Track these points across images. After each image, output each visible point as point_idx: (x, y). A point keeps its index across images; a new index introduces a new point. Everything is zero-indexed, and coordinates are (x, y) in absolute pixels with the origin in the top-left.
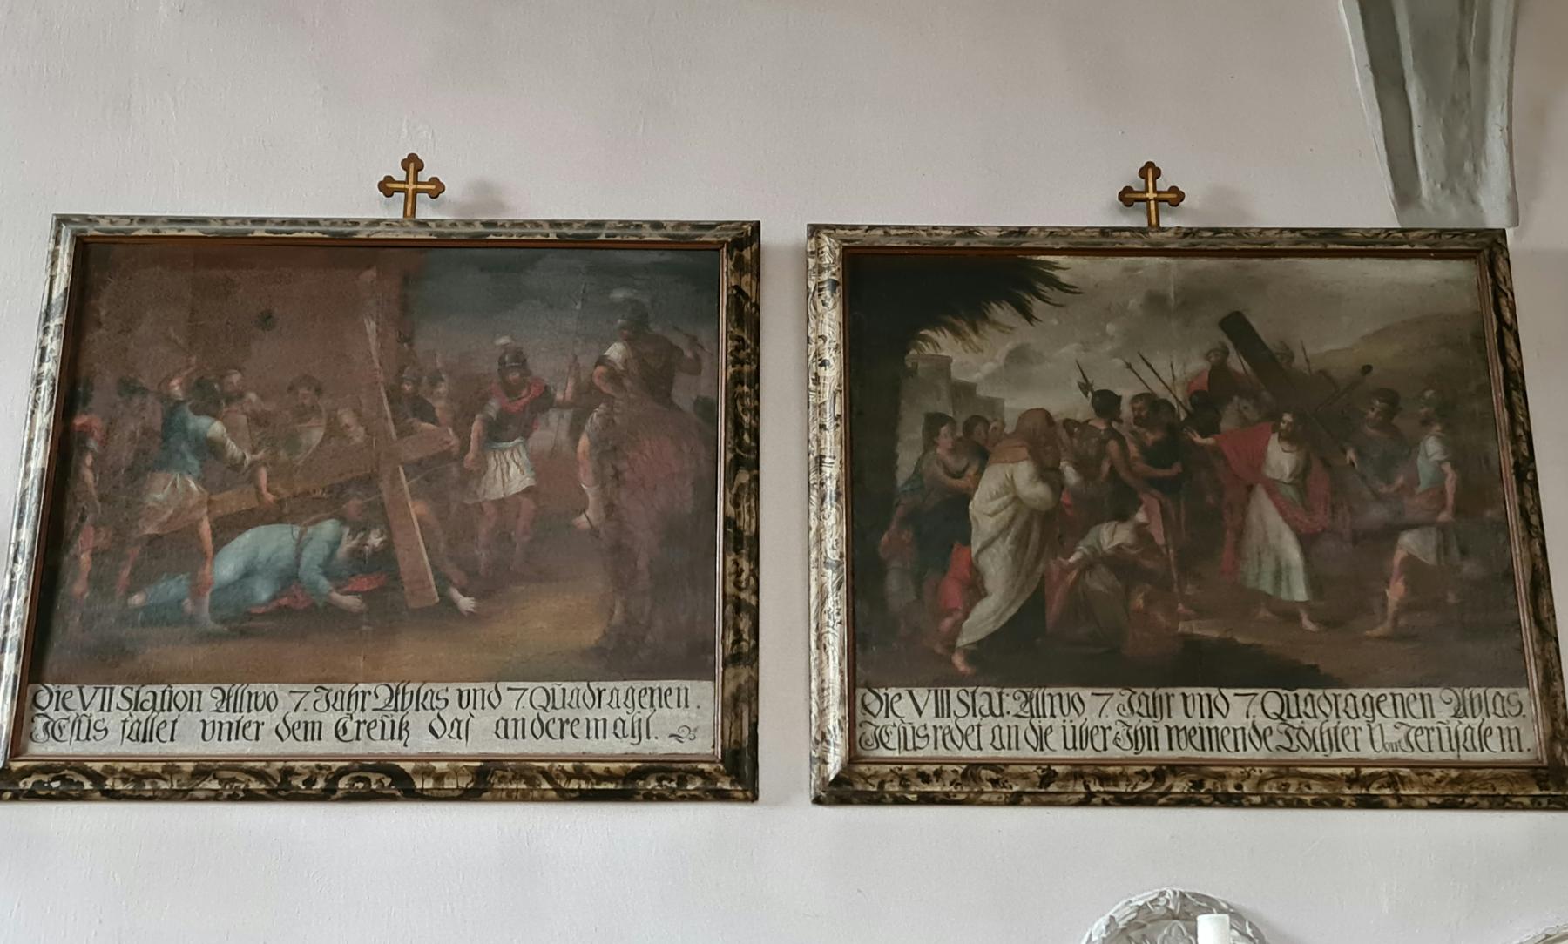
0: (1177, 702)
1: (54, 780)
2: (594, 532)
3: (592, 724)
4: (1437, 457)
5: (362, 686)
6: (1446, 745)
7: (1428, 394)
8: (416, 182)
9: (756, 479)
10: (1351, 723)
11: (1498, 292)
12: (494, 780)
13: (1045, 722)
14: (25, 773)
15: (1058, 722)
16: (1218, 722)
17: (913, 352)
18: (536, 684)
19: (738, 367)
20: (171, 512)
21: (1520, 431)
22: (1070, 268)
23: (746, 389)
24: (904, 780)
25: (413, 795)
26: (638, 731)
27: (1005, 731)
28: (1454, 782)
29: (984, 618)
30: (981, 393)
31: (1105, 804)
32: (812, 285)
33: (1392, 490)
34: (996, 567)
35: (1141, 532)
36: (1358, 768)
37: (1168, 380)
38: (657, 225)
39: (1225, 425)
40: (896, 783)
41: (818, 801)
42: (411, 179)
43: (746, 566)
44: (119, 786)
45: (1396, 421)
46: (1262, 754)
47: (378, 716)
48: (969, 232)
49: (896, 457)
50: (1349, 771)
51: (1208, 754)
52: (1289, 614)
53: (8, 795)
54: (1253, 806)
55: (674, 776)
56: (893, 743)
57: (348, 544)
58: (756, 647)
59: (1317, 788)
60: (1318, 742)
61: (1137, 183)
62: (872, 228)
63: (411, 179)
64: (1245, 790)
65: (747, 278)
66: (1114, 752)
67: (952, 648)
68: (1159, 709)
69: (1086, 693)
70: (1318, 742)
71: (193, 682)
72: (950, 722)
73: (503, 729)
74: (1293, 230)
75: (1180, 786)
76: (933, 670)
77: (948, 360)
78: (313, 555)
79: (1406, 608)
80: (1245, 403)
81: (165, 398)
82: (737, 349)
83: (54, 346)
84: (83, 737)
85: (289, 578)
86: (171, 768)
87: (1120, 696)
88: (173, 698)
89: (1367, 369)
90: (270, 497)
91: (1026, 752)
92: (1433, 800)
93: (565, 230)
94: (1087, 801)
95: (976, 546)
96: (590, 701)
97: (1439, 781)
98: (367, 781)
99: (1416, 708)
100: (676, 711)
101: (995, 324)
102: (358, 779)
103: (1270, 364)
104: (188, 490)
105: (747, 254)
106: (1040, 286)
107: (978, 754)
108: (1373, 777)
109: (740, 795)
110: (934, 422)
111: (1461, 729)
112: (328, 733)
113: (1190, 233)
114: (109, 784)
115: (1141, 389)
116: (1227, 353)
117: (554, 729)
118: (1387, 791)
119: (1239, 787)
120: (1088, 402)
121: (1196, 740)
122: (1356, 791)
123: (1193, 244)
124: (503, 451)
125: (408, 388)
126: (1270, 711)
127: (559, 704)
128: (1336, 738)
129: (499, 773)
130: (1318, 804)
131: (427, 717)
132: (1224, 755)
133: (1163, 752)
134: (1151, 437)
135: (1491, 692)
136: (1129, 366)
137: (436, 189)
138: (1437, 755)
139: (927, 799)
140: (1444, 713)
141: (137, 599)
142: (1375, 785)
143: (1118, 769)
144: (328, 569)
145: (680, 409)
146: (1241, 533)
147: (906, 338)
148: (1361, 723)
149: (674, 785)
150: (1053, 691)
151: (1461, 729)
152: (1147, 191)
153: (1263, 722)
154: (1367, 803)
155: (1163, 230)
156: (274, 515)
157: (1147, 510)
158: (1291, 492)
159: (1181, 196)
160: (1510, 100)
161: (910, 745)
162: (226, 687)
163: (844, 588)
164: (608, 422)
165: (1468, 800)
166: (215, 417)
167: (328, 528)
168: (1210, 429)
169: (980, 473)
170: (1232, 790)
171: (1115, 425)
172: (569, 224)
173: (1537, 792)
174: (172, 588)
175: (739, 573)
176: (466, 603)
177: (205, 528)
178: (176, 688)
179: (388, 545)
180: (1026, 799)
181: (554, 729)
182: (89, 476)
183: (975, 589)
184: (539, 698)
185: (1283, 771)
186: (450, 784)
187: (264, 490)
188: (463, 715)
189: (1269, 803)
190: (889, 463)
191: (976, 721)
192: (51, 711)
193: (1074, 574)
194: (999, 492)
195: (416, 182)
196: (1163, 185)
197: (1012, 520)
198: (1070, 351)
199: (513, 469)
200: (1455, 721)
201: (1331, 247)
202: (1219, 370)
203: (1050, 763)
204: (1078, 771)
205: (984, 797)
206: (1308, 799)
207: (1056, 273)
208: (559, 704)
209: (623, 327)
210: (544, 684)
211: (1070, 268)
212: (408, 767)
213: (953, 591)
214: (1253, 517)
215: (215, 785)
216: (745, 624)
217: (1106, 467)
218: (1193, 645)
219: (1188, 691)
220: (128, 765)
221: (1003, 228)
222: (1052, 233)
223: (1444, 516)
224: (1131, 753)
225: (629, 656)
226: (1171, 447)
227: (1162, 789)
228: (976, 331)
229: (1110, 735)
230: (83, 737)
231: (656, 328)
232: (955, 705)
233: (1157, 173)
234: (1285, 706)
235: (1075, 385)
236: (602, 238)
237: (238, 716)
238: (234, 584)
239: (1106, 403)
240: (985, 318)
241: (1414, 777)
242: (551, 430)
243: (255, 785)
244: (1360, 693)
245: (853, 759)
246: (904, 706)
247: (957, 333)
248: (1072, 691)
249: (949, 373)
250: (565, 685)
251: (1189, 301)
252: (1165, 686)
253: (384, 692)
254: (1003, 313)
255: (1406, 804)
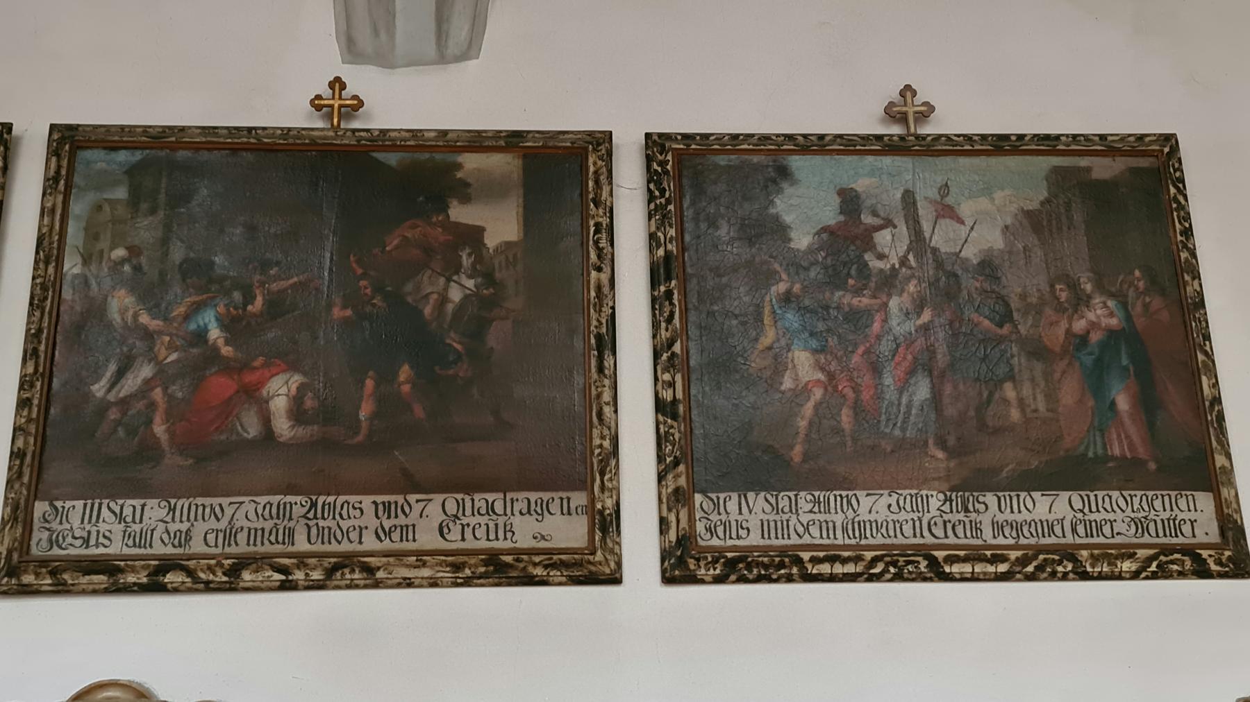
8: (340, 98)
60: (850, 532)
61: (920, 99)
63: (905, 108)
70: (850, 532)
160: (473, 25)
210: (456, 496)
233: (914, 93)
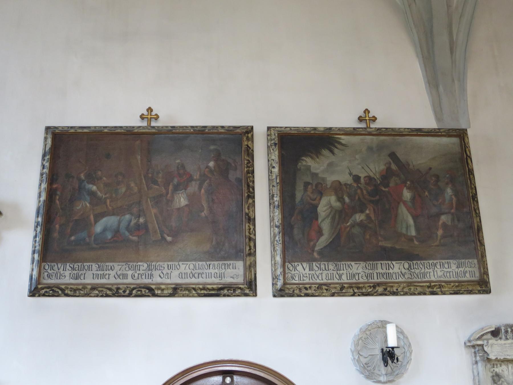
0: (379, 266)
1: (50, 291)
2: (206, 217)
3: (207, 274)
4: (450, 194)
5: (139, 263)
6: (454, 276)
7: (447, 176)
8: (151, 115)
9: (254, 202)
10: (428, 271)
11: (464, 146)
12: (179, 291)
13: (341, 272)
14: (42, 289)
15: (345, 272)
16: (391, 271)
17: (300, 164)
18: (190, 263)
19: (248, 169)
20: (82, 213)
21: (473, 186)
22: (344, 139)
23: (250, 175)
24: (300, 289)
25: (155, 295)
26: (221, 276)
27: (330, 275)
28: (457, 286)
29: (323, 242)
30: (320, 176)
31: (359, 295)
32: (269, 144)
33: (439, 203)
34: (326, 226)
35: (368, 216)
36: (430, 283)
37: (374, 172)
38: (223, 127)
39: (392, 184)
40: (298, 290)
41: (274, 296)
42: (149, 115)
43: (252, 227)
44: (69, 292)
45: (439, 183)
46: (404, 280)
47: (143, 272)
48: (315, 129)
49: (295, 195)
50: (428, 284)
51: (388, 280)
52: (410, 239)
53: (37, 295)
54: (401, 295)
55: (232, 289)
56: (297, 279)
57: (133, 222)
58: (255, 251)
59: (419, 289)
62: (286, 127)
63: (149, 115)
64: (399, 290)
65: (250, 142)
66: (361, 280)
67: (313, 251)
68: (374, 267)
69: (353, 263)
71: (89, 262)
72: (313, 272)
73: (181, 276)
74: (408, 129)
75: (380, 289)
76: (308, 257)
77: (310, 166)
78: (123, 225)
79: (444, 237)
80: (396, 178)
81: (79, 179)
82: (248, 163)
83: (47, 164)
84: (58, 278)
85: (117, 232)
86: (84, 286)
87: (363, 264)
88: (84, 267)
89: (430, 169)
90: (110, 208)
91: (336, 281)
92: (451, 292)
93: (195, 129)
94: (353, 295)
95: (320, 220)
96: (207, 268)
97: (453, 286)
98: (141, 291)
99: (446, 266)
100: (232, 270)
101: (323, 155)
102: (139, 291)
103: (403, 166)
104: (86, 206)
105: (250, 135)
106: (336, 144)
107: (322, 282)
108: (435, 286)
109: (252, 295)
110: (306, 184)
111: (459, 271)
112: (130, 277)
113: (379, 129)
114: (66, 292)
115: (366, 174)
116: (390, 164)
117: (196, 275)
118: (439, 290)
119: (397, 290)
120: (351, 178)
121: (385, 276)
122: (430, 290)
123: (381, 132)
124: (179, 194)
125: (150, 175)
126: (405, 267)
127: (197, 268)
128: (424, 275)
129: (180, 289)
130: (419, 294)
131: (159, 272)
132: (393, 280)
133: (376, 280)
134: (370, 188)
135: (467, 261)
136: (363, 168)
137: (157, 117)
138: (452, 279)
139: (307, 295)
140: (454, 267)
141: (73, 238)
142: (435, 288)
143: (362, 285)
144: (128, 228)
145: (230, 181)
146: (396, 216)
147: (297, 159)
148: (431, 270)
149: (232, 292)
150: (343, 263)
151: (459, 271)
152: (366, 117)
153: (404, 271)
154: (433, 293)
155: (371, 128)
156: (113, 214)
157: (369, 210)
158: (410, 204)
159: (376, 119)
160: (473, 14)
161: (302, 279)
162: (99, 264)
163: (281, 233)
164: (210, 185)
165: (461, 292)
166: (94, 184)
167: (128, 217)
168: (387, 186)
169: (320, 199)
170: (395, 290)
171: (359, 185)
172: (197, 127)
173: (479, 289)
174: (83, 235)
175: (250, 229)
176: (169, 239)
177: (92, 217)
178: (85, 264)
179: (146, 222)
180: (336, 295)
181: (196, 275)
182: (58, 202)
183: (320, 233)
184: (192, 267)
185: (410, 284)
186: (166, 292)
187: (108, 206)
188: (169, 272)
189: (406, 294)
190: (293, 196)
191: (321, 272)
192: (49, 271)
193: (348, 229)
194: (327, 204)
195: (151, 115)
196: (371, 115)
197: (330, 212)
198: (345, 164)
199: (182, 199)
200: (457, 270)
201: (419, 133)
202: (389, 169)
203: (343, 283)
204: (351, 286)
205: (324, 294)
206: (416, 293)
207: (341, 141)
208: (197, 268)
209: (213, 157)
211: (344, 139)
212: (153, 287)
213: (313, 234)
214: (400, 211)
215: (97, 292)
216: (252, 244)
217: (357, 198)
218: (384, 249)
219: (382, 262)
220: (72, 286)
221: (325, 128)
222: (339, 129)
223: (453, 211)
224: (366, 281)
225: (218, 253)
226: (376, 191)
227: (375, 291)
228: (318, 158)
229: (360, 275)
230: (58, 278)
231: (223, 157)
232: (315, 267)
233: (369, 112)
234: (410, 266)
235: (347, 173)
236: (207, 131)
237: (103, 272)
238: (100, 233)
239: (357, 179)
240: (320, 154)
241: (446, 286)
242: (193, 187)
243: (109, 292)
244: (431, 262)
245: (285, 284)
246: (300, 268)
247: (312, 158)
248: (349, 263)
249: (310, 170)
250: (199, 263)
251: (381, 148)
252: (375, 261)
253: (146, 265)
254: (326, 152)
255: (444, 293)
